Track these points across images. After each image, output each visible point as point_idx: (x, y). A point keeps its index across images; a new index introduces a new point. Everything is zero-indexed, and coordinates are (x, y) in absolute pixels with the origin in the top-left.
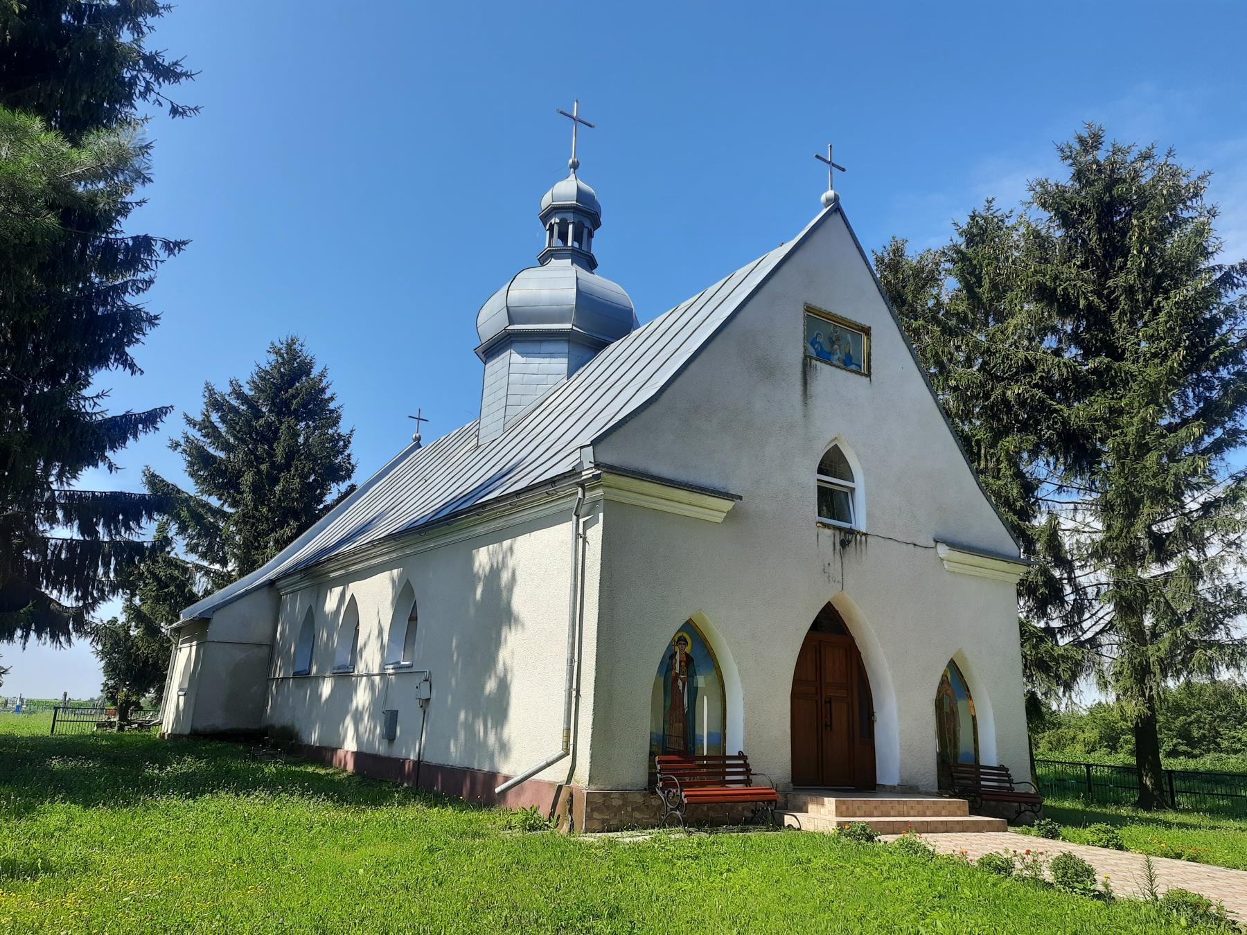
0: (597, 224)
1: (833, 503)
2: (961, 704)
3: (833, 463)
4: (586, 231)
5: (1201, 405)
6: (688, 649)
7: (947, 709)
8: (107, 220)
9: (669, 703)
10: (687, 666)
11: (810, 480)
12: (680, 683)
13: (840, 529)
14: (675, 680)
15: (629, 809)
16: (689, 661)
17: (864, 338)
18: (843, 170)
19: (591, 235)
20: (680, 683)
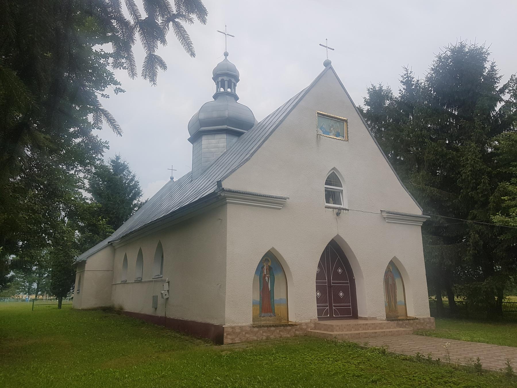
0: (238, 80)
1: (332, 196)
2: (398, 281)
3: (333, 179)
4: (233, 84)
5: (37, 21)
6: (269, 264)
7: (390, 282)
8: (507, 368)
9: (262, 288)
10: (270, 270)
11: (321, 187)
12: (267, 278)
13: (336, 208)
14: (264, 277)
15: (244, 333)
16: (270, 269)
17: (345, 123)
18: (320, 45)
19: (235, 85)
20: (267, 278)
